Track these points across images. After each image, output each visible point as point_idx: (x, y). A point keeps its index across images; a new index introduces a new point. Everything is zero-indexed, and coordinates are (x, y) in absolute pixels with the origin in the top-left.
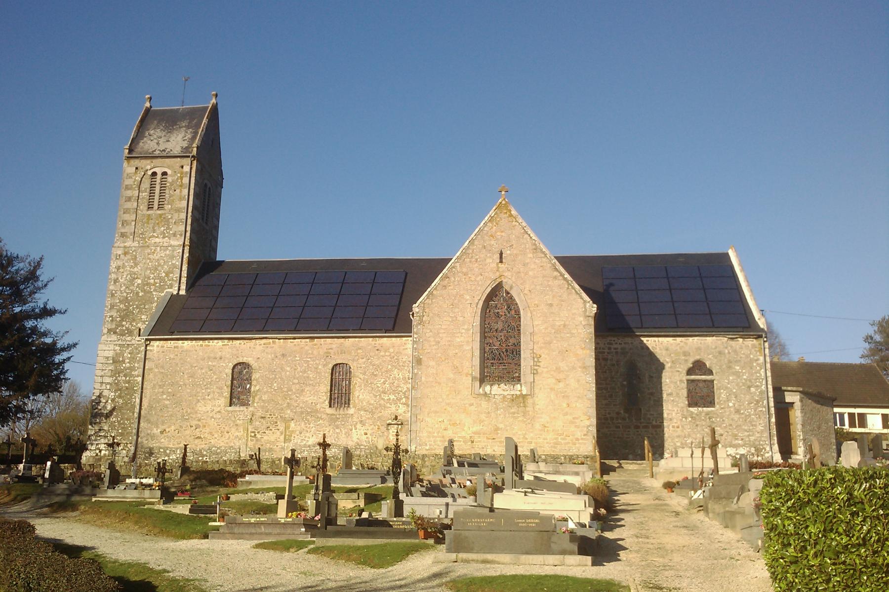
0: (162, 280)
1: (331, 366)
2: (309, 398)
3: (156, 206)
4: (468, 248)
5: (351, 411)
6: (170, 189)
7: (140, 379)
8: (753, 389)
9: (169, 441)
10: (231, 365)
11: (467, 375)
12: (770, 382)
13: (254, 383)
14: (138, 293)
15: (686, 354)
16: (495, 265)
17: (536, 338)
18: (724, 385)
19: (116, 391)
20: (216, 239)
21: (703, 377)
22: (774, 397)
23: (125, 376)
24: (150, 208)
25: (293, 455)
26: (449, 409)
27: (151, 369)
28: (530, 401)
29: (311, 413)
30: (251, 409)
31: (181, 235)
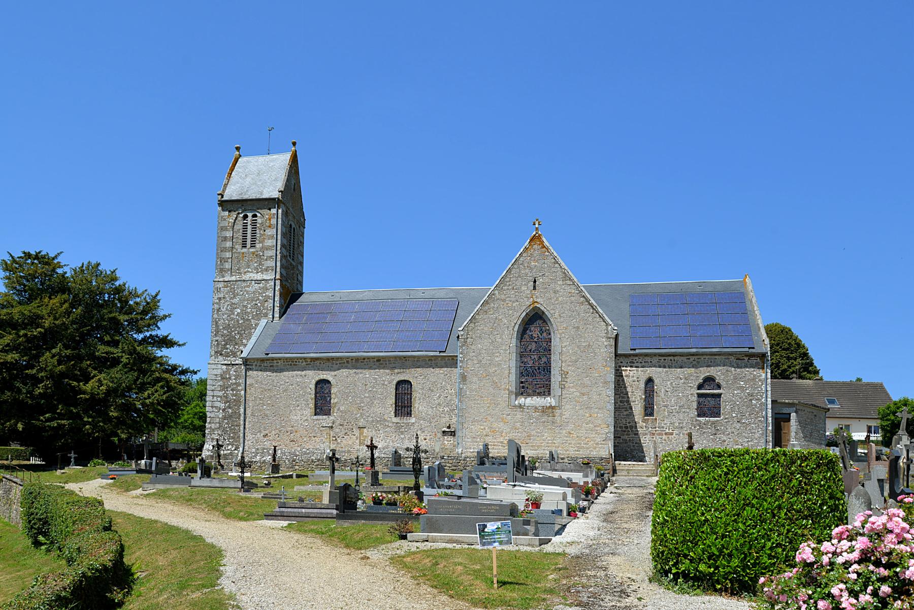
1: (395, 382)
3: (249, 245)
4: (506, 275)
5: (413, 420)
6: (260, 229)
7: (243, 392)
9: (256, 445)
10: (314, 382)
11: (504, 390)
12: (769, 396)
13: (333, 396)
14: (238, 321)
16: (529, 292)
17: (564, 358)
19: (225, 403)
20: (301, 273)
22: (772, 409)
23: (232, 390)
25: (334, 454)
26: (489, 418)
27: (251, 385)
30: (331, 418)
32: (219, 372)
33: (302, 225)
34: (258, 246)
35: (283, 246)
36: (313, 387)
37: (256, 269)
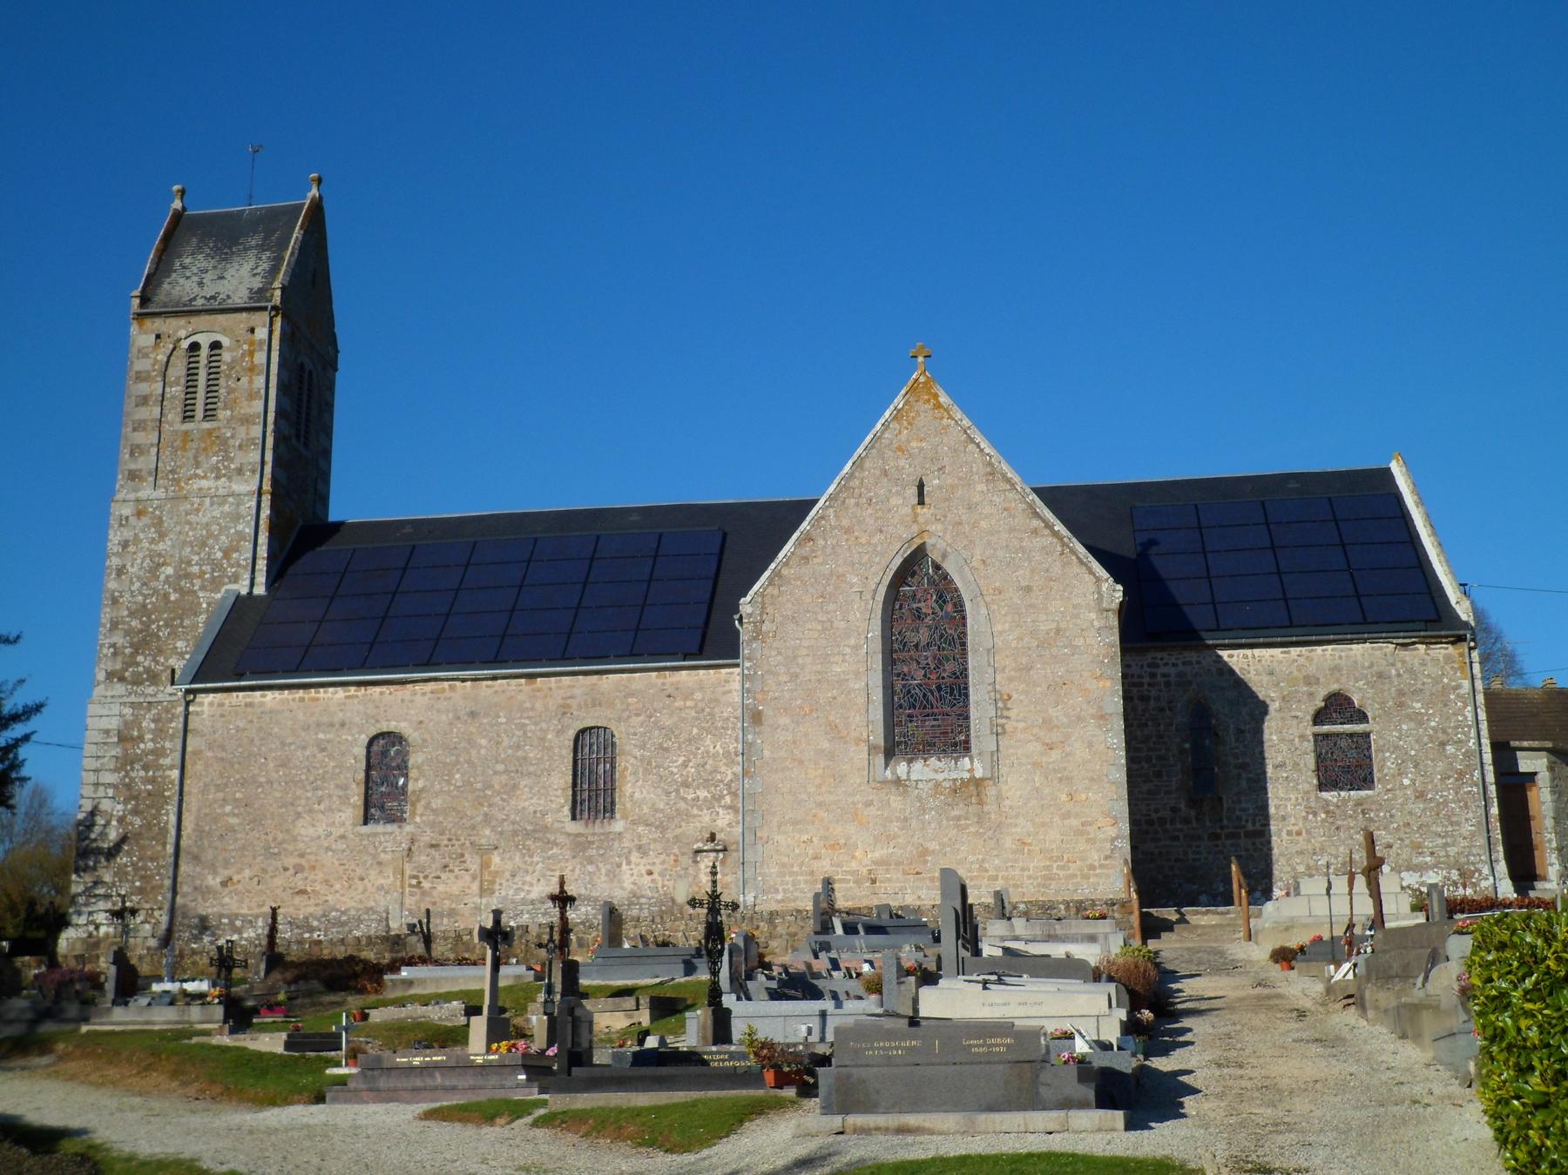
0: (216, 565)
1: (572, 733)
2: (528, 801)
3: (199, 413)
4: (851, 475)
5: (618, 825)
6: (228, 377)
7: (175, 774)
8: (1450, 749)
10: (364, 739)
11: (858, 741)
13: (413, 773)
14: (166, 596)
15: (1309, 680)
18: (1390, 742)
19: (126, 802)
21: (1348, 728)
23: (146, 768)
24: (188, 416)
25: (497, 921)
26: (822, 814)
27: (197, 753)
28: (990, 791)
29: (535, 833)
30: (408, 828)
31: (253, 471)
32: (114, 724)
33: (331, 364)
34: (223, 414)
35: (280, 413)
36: (361, 751)
37: (216, 469)
